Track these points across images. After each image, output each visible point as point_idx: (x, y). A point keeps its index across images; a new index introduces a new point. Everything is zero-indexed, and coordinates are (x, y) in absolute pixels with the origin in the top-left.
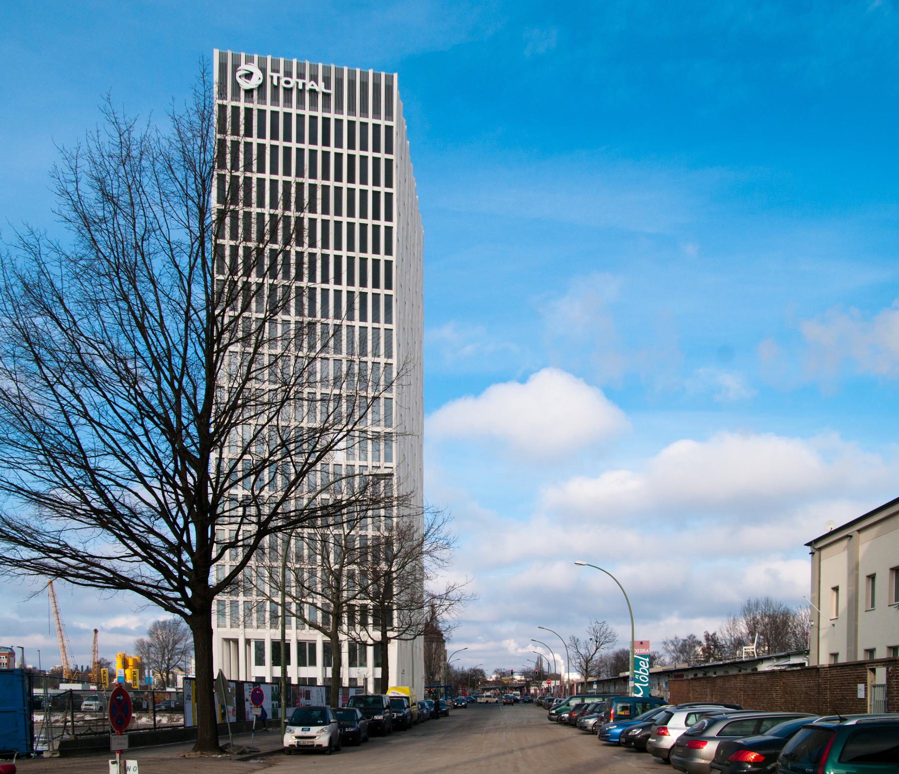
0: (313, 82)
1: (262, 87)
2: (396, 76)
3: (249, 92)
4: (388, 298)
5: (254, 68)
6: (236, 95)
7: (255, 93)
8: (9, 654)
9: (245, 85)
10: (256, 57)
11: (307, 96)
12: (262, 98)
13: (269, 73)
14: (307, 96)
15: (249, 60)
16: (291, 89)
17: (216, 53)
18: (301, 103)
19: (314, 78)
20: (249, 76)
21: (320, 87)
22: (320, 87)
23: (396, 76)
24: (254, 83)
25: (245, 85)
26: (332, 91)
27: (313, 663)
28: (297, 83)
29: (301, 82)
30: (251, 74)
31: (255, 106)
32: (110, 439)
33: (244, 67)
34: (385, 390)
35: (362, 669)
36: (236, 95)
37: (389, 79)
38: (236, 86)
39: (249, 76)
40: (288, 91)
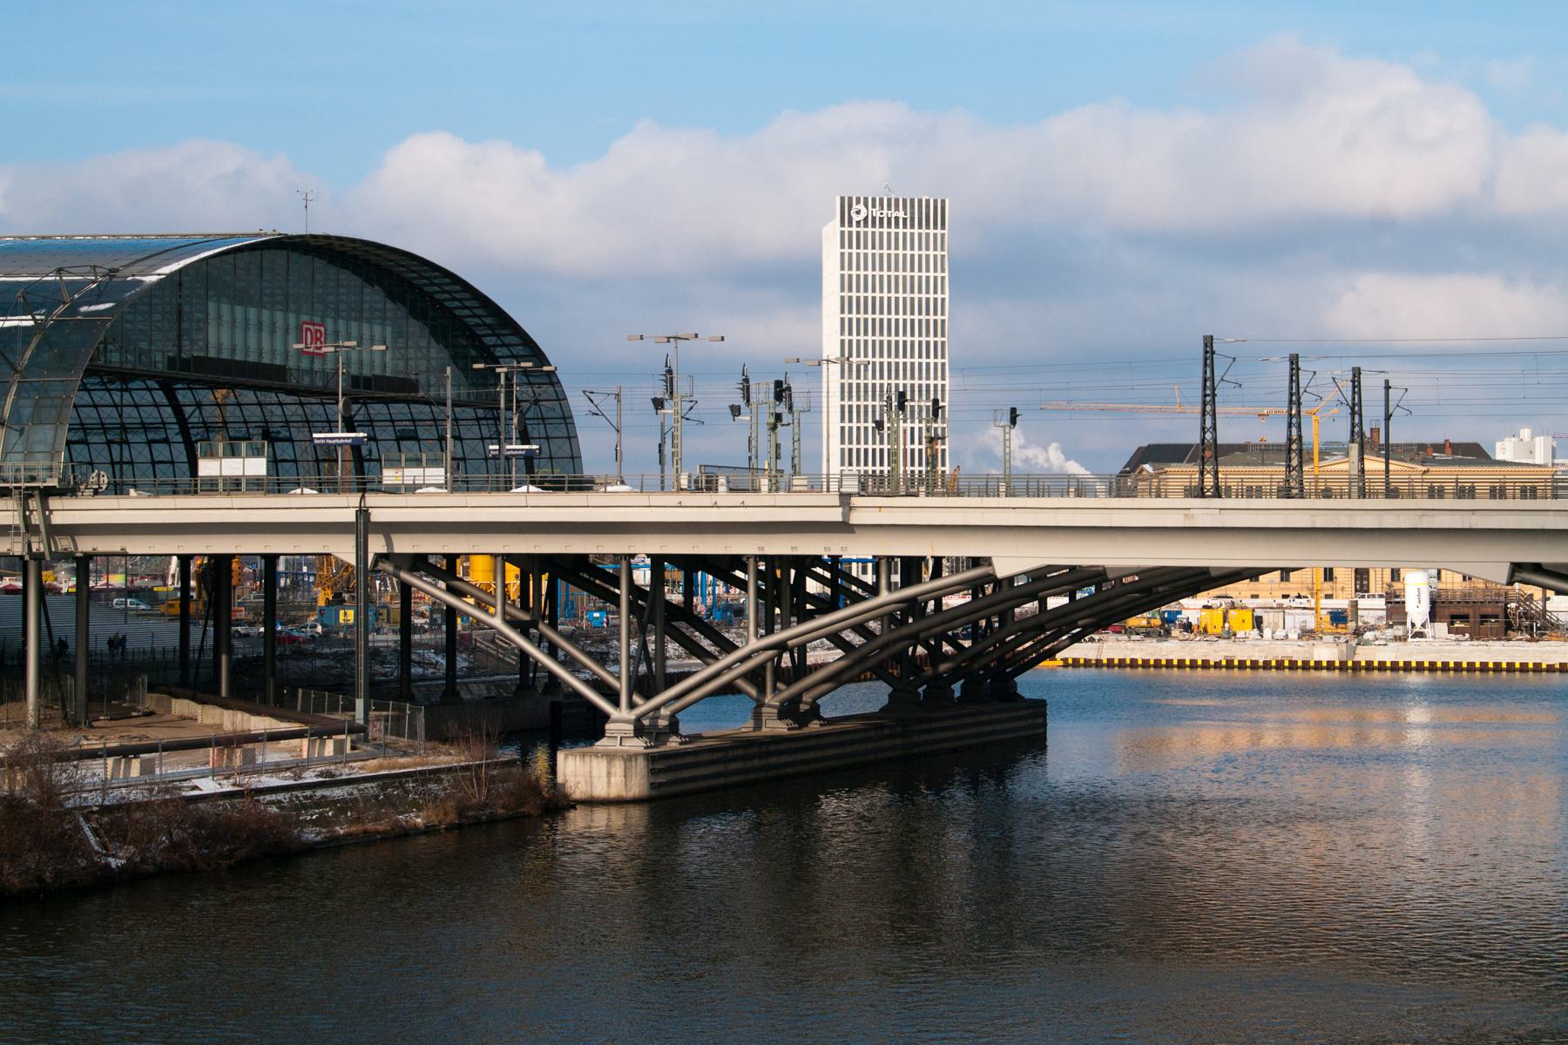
5: (861, 207)
6: (850, 225)
12: (866, 225)
20: (858, 212)
21: (901, 214)
22: (901, 214)
24: (861, 217)
25: (856, 218)
38: (850, 219)
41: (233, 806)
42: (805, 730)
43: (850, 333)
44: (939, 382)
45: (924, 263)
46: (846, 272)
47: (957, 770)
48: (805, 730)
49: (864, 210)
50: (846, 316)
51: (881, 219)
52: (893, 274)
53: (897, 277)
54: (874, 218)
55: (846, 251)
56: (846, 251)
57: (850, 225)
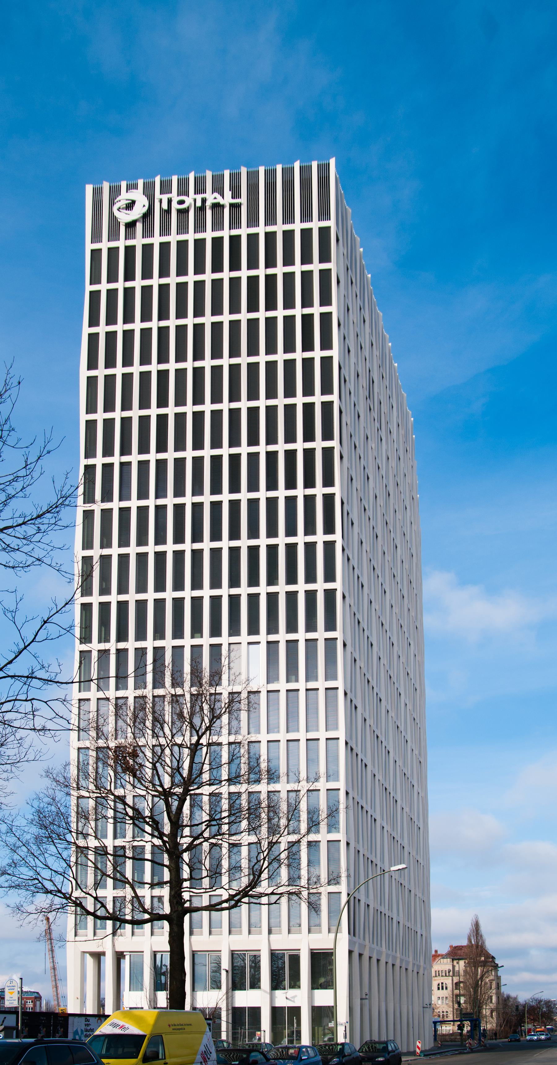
0: (216, 195)
1: (147, 216)
2: (332, 162)
3: (131, 225)
4: (328, 452)
5: (139, 196)
7: (139, 226)
8: (36, 998)
9: (124, 217)
10: (141, 183)
11: (209, 213)
13: (157, 195)
14: (209, 213)
15: (132, 187)
16: (186, 211)
17: (89, 189)
18: (200, 226)
19: (218, 189)
20: (130, 205)
23: (332, 162)
26: (243, 200)
27: (255, 984)
28: (195, 200)
29: (199, 197)
30: (133, 202)
31: (138, 242)
32: (406, 1039)
33: (125, 197)
34: (309, 831)
35: (291, 992)
36: (114, 235)
37: (324, 170)
39: (130, 205)
40: (183, 213)
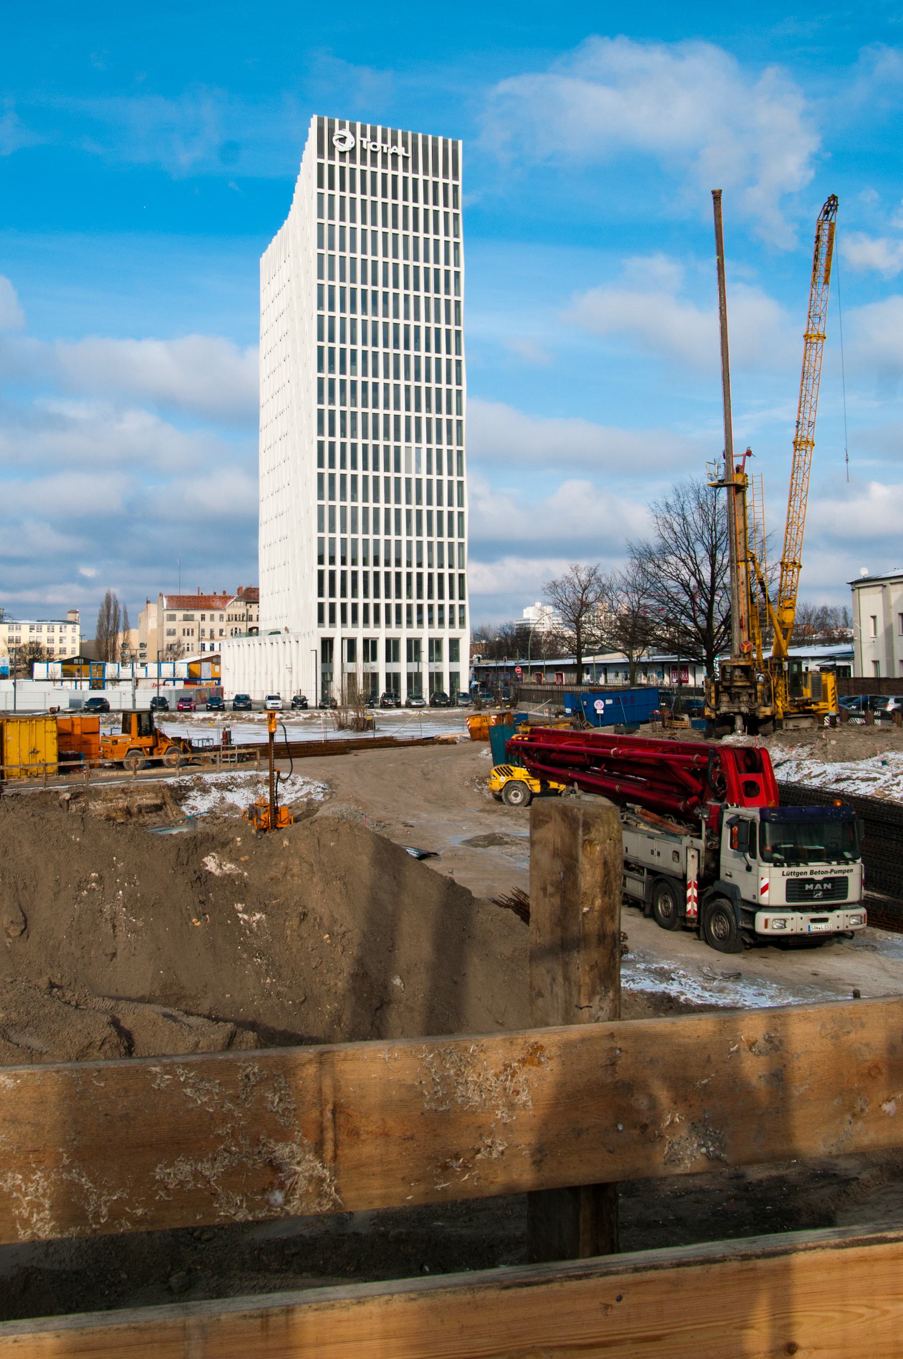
5: (346, 133)
6: (331, 156)
12: (353, 160)
20: (343, 140)
21: (400, 150)
22: (400, 150)
24: (347, 147)
25: (339, 147)
38: (332, 147)
41: (739, 708)
42: (713, 742)
43: (332, 433)
44: (454, 387)
45: (433, 222)
46: (327, 567)
47: (329, 941)
48: (713, 742)
49: (350, 138)
50: (326, 375)
51: (374, 153)
52: (370, 442)
53: (376, 479)
54: (364, 151)
55: (326, 471)
56: (326, 471)
57: (331, 156)
